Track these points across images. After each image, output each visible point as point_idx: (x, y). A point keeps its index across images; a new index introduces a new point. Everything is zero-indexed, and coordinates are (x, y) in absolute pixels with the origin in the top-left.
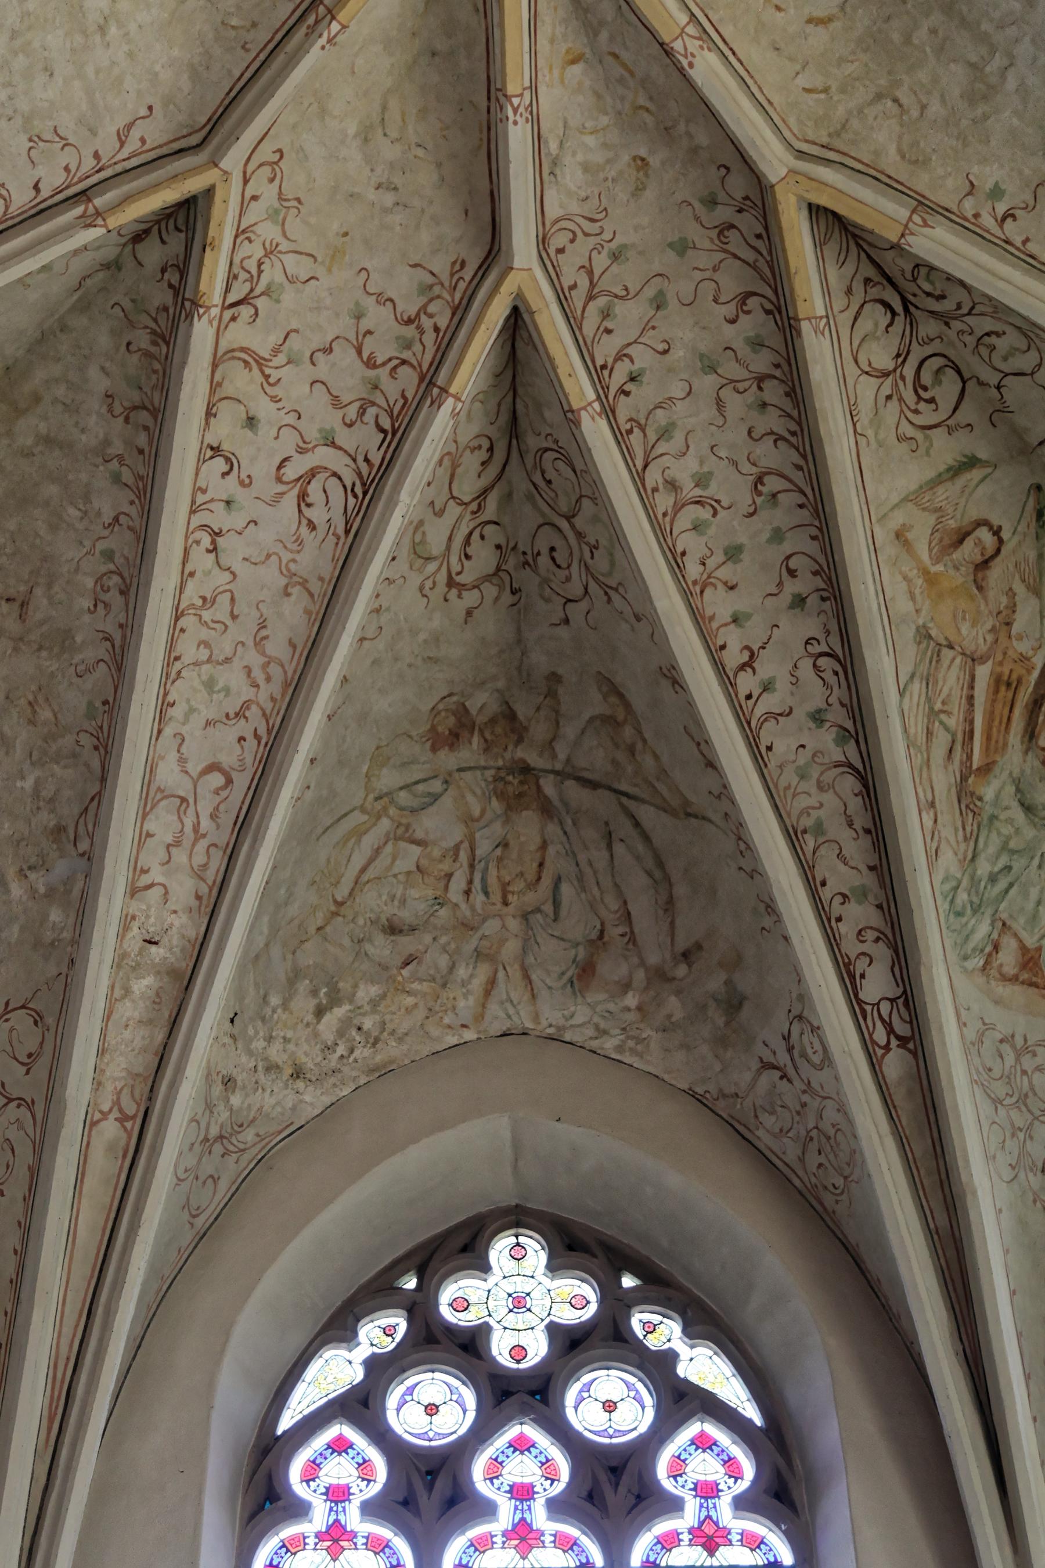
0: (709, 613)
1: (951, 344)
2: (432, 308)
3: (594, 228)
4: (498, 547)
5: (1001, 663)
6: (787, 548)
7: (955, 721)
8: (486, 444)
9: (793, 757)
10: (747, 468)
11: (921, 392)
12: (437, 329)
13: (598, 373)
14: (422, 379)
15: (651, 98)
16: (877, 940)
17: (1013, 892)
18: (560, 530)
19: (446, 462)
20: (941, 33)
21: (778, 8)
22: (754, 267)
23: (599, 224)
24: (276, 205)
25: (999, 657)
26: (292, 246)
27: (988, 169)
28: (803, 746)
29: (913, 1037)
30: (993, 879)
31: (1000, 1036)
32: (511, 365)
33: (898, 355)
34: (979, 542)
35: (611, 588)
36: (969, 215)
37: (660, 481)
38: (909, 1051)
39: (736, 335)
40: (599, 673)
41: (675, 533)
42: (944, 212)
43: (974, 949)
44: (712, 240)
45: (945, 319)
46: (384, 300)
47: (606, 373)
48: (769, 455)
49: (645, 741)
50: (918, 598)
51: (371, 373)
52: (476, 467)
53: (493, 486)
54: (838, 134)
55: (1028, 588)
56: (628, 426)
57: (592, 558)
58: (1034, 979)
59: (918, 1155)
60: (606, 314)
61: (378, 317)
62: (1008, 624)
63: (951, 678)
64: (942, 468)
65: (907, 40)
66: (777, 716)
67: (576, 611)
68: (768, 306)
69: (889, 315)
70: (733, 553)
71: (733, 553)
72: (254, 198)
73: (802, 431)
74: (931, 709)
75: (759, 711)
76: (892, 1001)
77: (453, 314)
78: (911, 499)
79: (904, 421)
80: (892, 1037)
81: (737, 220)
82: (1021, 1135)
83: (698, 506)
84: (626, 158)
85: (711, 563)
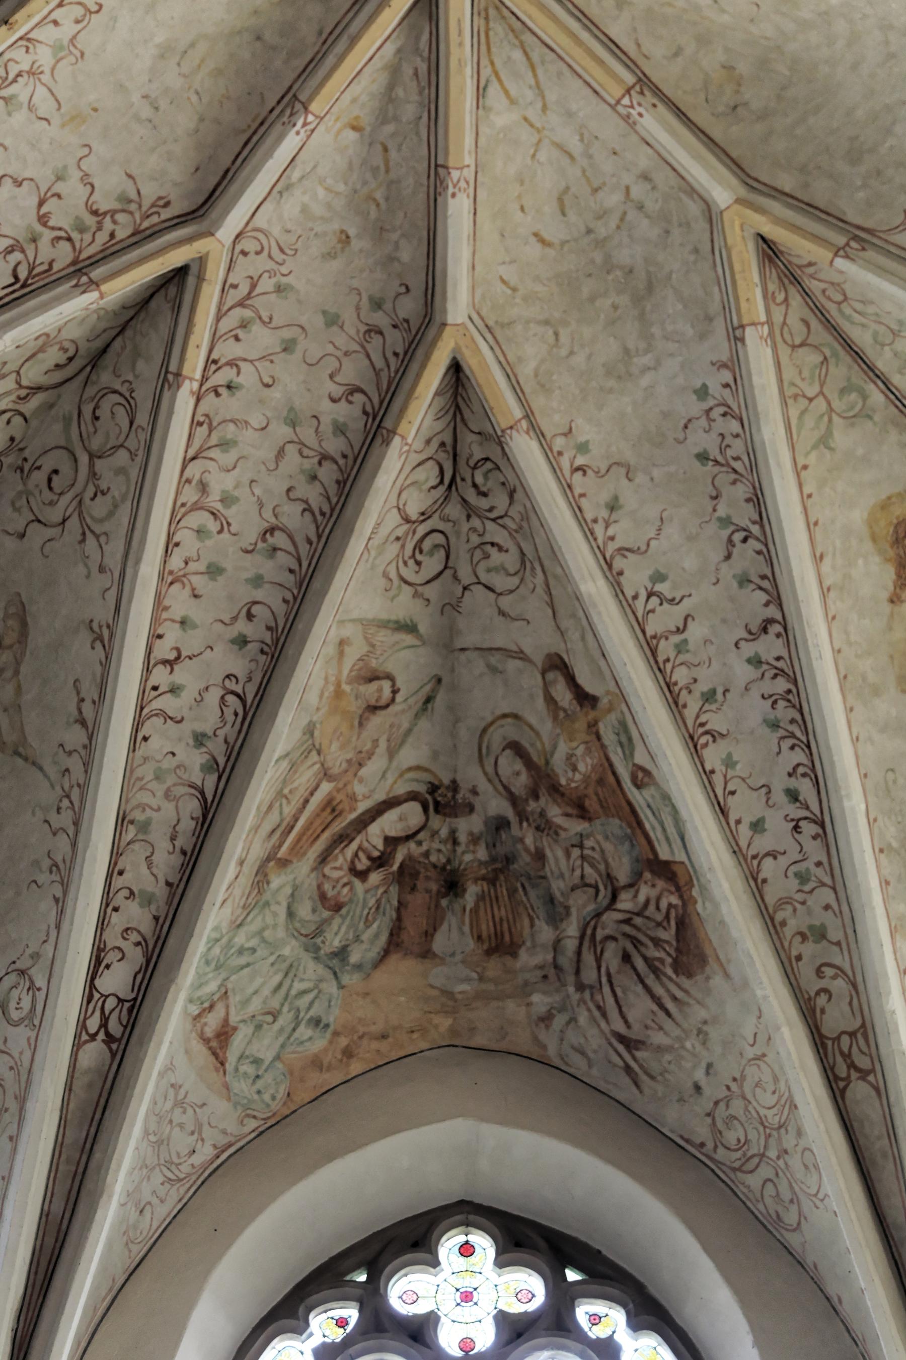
0: (166, 602)
1: (458, 534)
2: (119, 217)
3: (279, 257)
4: (12, 439)
5: (338, 791)
6: (259, 595)
7: (289, 810)
8: (71, 353)
9: (159, 757)
10: (268, 514)
11: (417, 551)
12: (112, 235)
13: (211, 362)
14: (74, 262)
15: (387, 199)
16: (138, 944)
17: (246, 971)
18: (76, 461)
19: (40, 342)
20: (619, 311)
21: (522, 209)
22: (377, 373)
23: (284, 257)
24: (66, 42)
25: (341, 785)
26: (51, 84)
28: (173, 754)
29: (119, 1040)
30: (241, 951)
31: (173, 1081)
32: (138, 307)
33: (423, 514)
34: (380, 690)
35: (92, 532)
36: (556, 449)
37: (197, 477)
38: (110, 1049)
39: (330, 412)
40: (19, 594)
41: (182, 524)
42: (540, 435)
43: (199, 998)
44: (358, 331)
45: (470, 511)
46: (86, 180)
47: (214, 367)
48: (292, 516)
49: (17, 672)
50: (324, 700)
51: (39, 228)
52: (50, 363)
53: (47, 389)
54: (503, 326)
55: (388, 748)
56: (202, 419)
57: (92, 499)
58: (218, 1051)
59: (66, 1141)
60: (244, 325)
61: (73, 189)
62: (361, 765)
63: (305, 777)
64: (393, 618)
65: (592, 299)
66: (167, 717)
67: (37, 535)
68: (369, 409)
69: (438, 480)
70: (214, 571)
71: (214, 571)
72: (56, 23)
73: (331, 516)
74: (282, 789)
75: (156, 705)
76: (120, 1001)
77: (133, 235)
78: (365, 623)
79: (394, 564)
80: (103, 1030)
81: (388, 331)
82: (145, 1171)
83: (212, 517)
84: (336, 226)
85: (193, 566)
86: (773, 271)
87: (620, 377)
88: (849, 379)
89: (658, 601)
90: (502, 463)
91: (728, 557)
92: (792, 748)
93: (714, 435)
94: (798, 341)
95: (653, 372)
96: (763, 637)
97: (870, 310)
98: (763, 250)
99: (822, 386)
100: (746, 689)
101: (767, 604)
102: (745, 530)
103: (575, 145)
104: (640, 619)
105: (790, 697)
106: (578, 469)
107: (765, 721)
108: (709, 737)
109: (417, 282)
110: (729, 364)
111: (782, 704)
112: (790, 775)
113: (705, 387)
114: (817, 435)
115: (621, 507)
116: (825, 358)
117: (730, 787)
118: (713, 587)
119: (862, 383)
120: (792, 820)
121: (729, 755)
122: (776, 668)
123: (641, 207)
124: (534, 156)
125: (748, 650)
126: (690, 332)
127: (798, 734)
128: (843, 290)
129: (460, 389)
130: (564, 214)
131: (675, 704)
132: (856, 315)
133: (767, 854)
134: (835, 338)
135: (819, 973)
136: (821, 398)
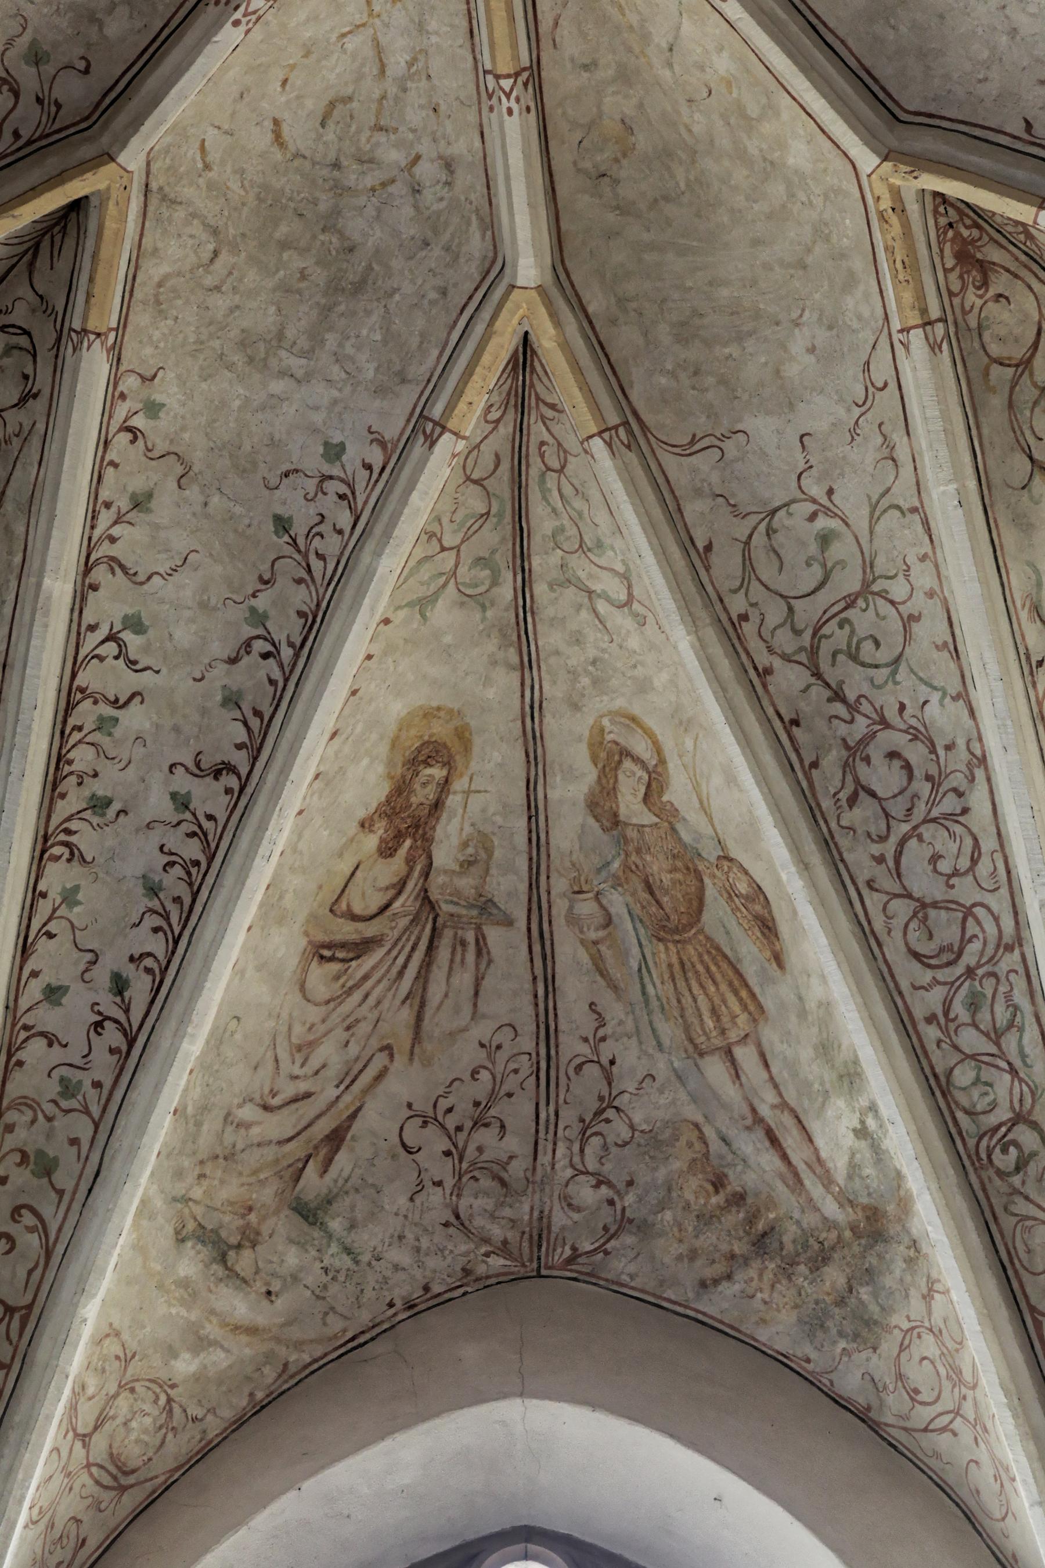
20: (303, 285)
21: (285, 82)
27: (176, 389)
54: (164, 198)
65: (284, 245)
86: (509, 381)
87: (251, 360)
88: (493, 552)
89: (116, 652)
90: (44, 356)
91: (233, 661)
92: (156, 930)
93: (312, 510)
94: (475, 476)
95: (292, 383)
96: (209, 780)
97: (578, 504)
98: (516, 351)
99: (463, 542)
100: (148, 826)
101: (239, 747)
102: (274, 644)
103: (397, 62)
104: (80, 658)
105: (194, 871)
106: (129, 429)
107: (144, 877)
108: (66, 852)
109: (107, 71)
110: (389, 445)
111: (177, 871)
112: (132, 959)
113: (341, 448)
114: (422, 592)
115: (149, 511)
116: (488, 513)
117: (52, 927)
118: (191, 682)
119: (503, 565)
120: (100, 1013)
121: (76, 889)
122: (200, 826)
123: (416, 190)
124: (344, 35)
125: (182, 782)
126: (369, 372)
127: (174, 919)
128: (566, 461)
129: (57, 229)
130: (323, 125)
131: (53, 787)
132: (555, 493)
133: (43, 1034)
134: (513, 498)
135: (16, 1213)
136: (454, 552)
